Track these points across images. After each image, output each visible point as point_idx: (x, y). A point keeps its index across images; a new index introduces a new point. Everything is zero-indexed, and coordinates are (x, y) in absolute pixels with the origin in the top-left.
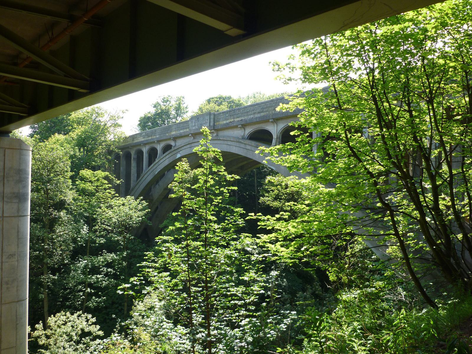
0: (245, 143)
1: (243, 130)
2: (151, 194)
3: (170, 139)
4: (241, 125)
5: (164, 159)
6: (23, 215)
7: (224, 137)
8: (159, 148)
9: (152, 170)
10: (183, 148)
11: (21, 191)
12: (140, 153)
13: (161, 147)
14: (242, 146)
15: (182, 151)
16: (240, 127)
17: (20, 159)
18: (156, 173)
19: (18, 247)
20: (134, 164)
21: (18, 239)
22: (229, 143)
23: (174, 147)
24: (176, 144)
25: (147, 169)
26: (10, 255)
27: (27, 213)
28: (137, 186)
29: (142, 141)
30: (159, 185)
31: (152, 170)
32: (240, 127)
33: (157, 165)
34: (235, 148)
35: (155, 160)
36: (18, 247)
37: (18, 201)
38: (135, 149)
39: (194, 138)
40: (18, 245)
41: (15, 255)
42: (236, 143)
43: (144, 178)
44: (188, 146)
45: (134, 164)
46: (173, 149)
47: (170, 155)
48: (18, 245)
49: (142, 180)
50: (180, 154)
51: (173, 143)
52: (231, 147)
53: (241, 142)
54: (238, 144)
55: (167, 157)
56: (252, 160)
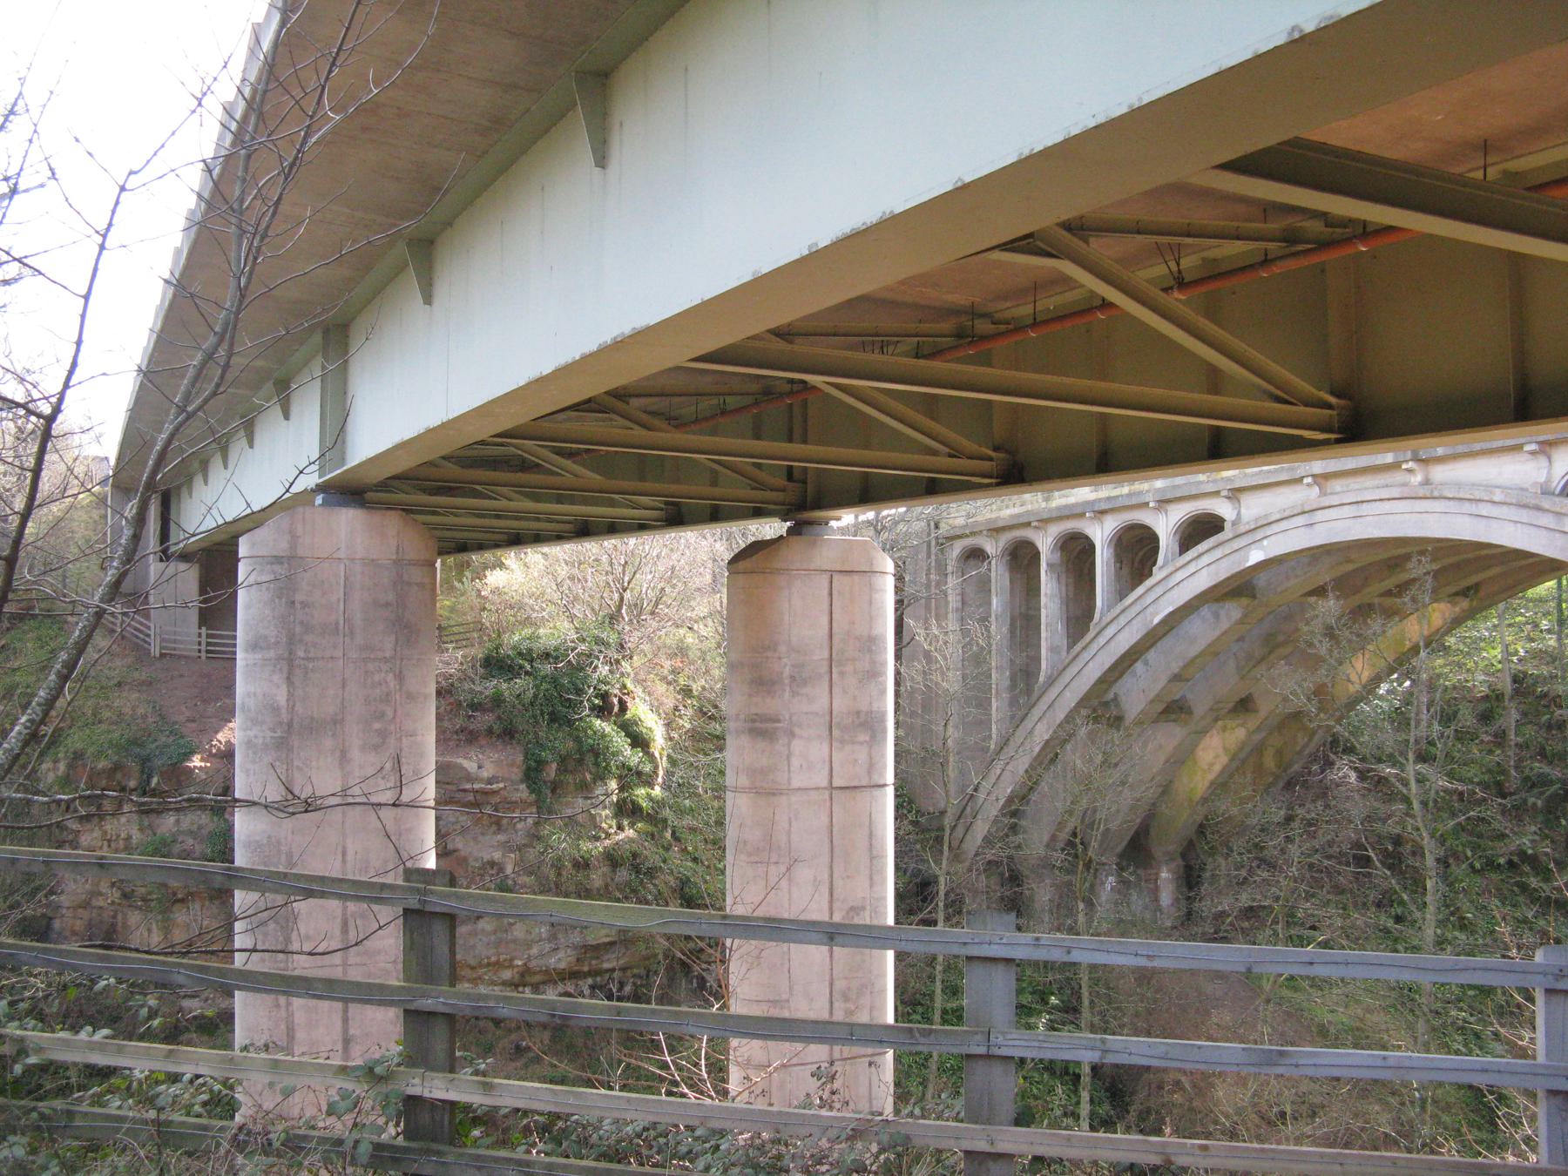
0: (1558, 509)
1: (1543, 461)
2: (1110, 696)
3: (1217, 493)
4: (1538, 443)
5: (1192, 568)
6: (882, 782)
7: (1459, 485)
8: (1165, 526)
9: (1137, 608)
10: (1269, 530)
11: (875, 709)
12: (1077, 551)
13: (1172, 524)
14: (1547, 520)
15: (1273, 538)
16: (1533, 453)
17: (870, 603)
18: (1156, 620)
19: (871, 886)
20: (1049, 587)
21: (872, 859)
22: (1485, 509)
23: (1234, 523)
24: (1239, 514)
25: (1110, 607)
26: (852, 908)
27: (882, 774)
28: (1073, 670)
29: (1088, 503)
30: (1146, 663)
31: (1137, 608)
32: (1533, 453)
33: (1159, 590)
34: (1510, 528)
35: (1150, 574)
36: (871, 886)
37: (867, 738)
38: (1055, 530)
39: (1323, 493)
40: (871, 879)
41: (863, 908)
42: (1513, 509)
43: (1102, 640)
44: (1300, 520)
45: (1049, 587)
46: (1227, 533)
47: (1218, 553)
48: (871, 879)
49: (1095, 647)
50: (1262, 548)
51: (1224, 509)
52: (1494, 523)
53: (1538, 508)
54: (1524, 515)
55: (1206, 559)
56: (1499, 550)
